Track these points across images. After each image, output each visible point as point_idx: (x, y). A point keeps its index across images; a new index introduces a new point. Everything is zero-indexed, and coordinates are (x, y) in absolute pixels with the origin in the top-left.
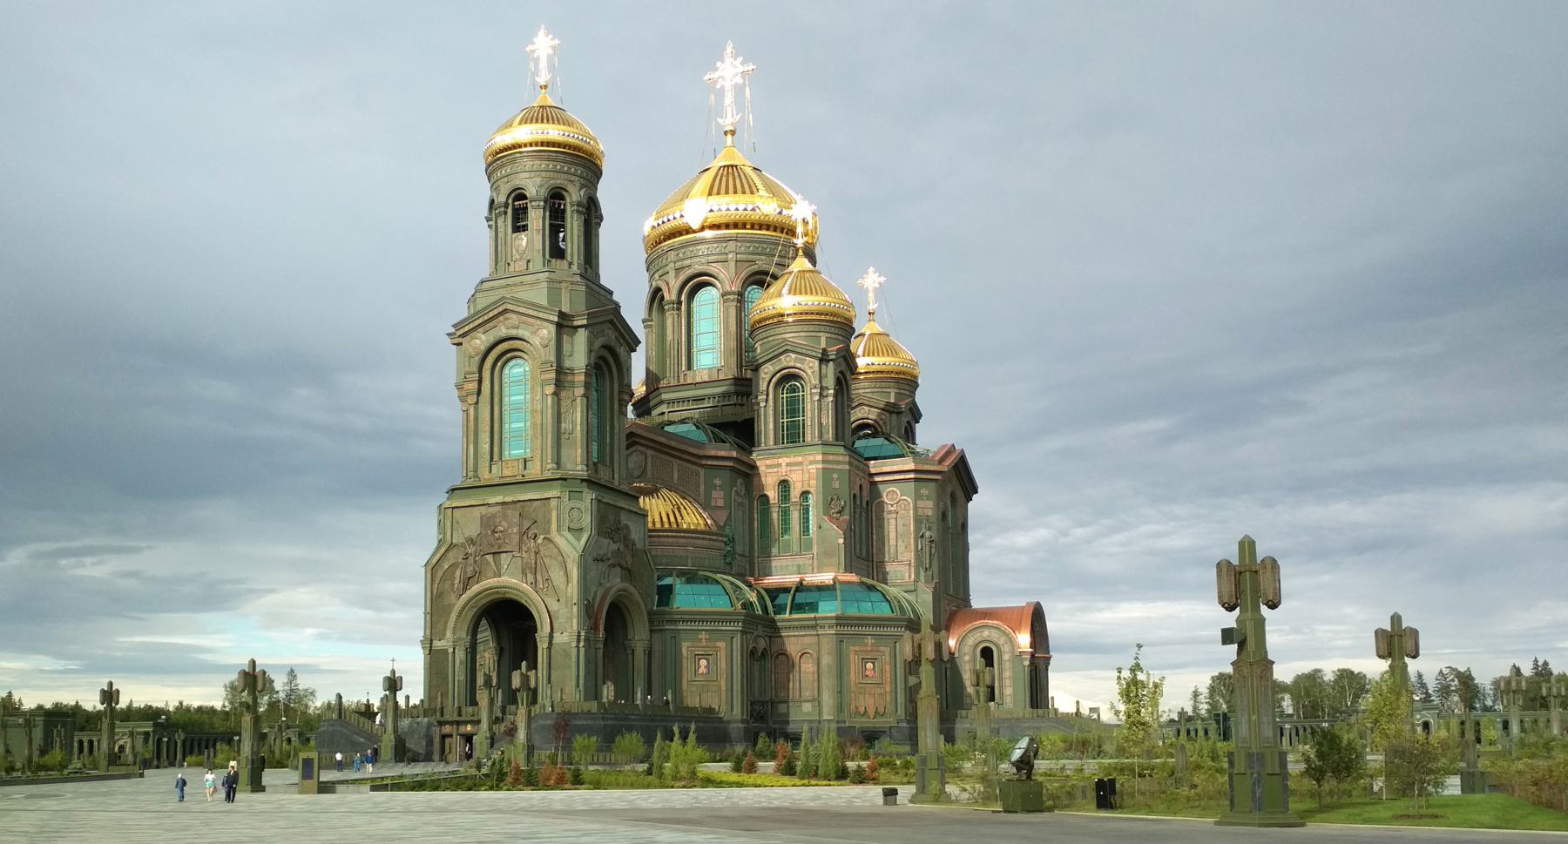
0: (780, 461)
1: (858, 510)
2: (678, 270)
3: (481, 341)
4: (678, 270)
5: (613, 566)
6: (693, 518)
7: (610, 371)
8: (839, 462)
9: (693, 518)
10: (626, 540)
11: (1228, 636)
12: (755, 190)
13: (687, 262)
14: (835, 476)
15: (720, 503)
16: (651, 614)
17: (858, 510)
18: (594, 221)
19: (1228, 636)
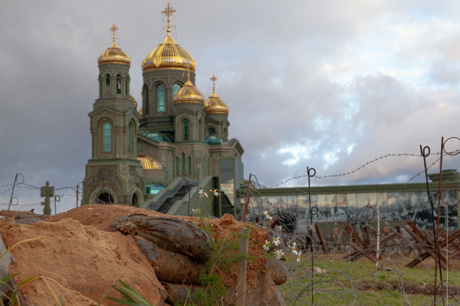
0: (182, 146)
1: (205, 162)
2: (153, 79)
3: (99, 117)
4: (153, 79)
5: (134, 183)
6: (156, 166)
7: (133, 126)
8: (196, 147)
9: (156, 166)
10: (137, 176)
11: (42, 204)
12: (176, 54)
13: (155, 77)
14: (198, 152)
15: (164, 160)
16: (144, 196)
17: (205, 162)
18: (128, 81)
19: (42, 204)
